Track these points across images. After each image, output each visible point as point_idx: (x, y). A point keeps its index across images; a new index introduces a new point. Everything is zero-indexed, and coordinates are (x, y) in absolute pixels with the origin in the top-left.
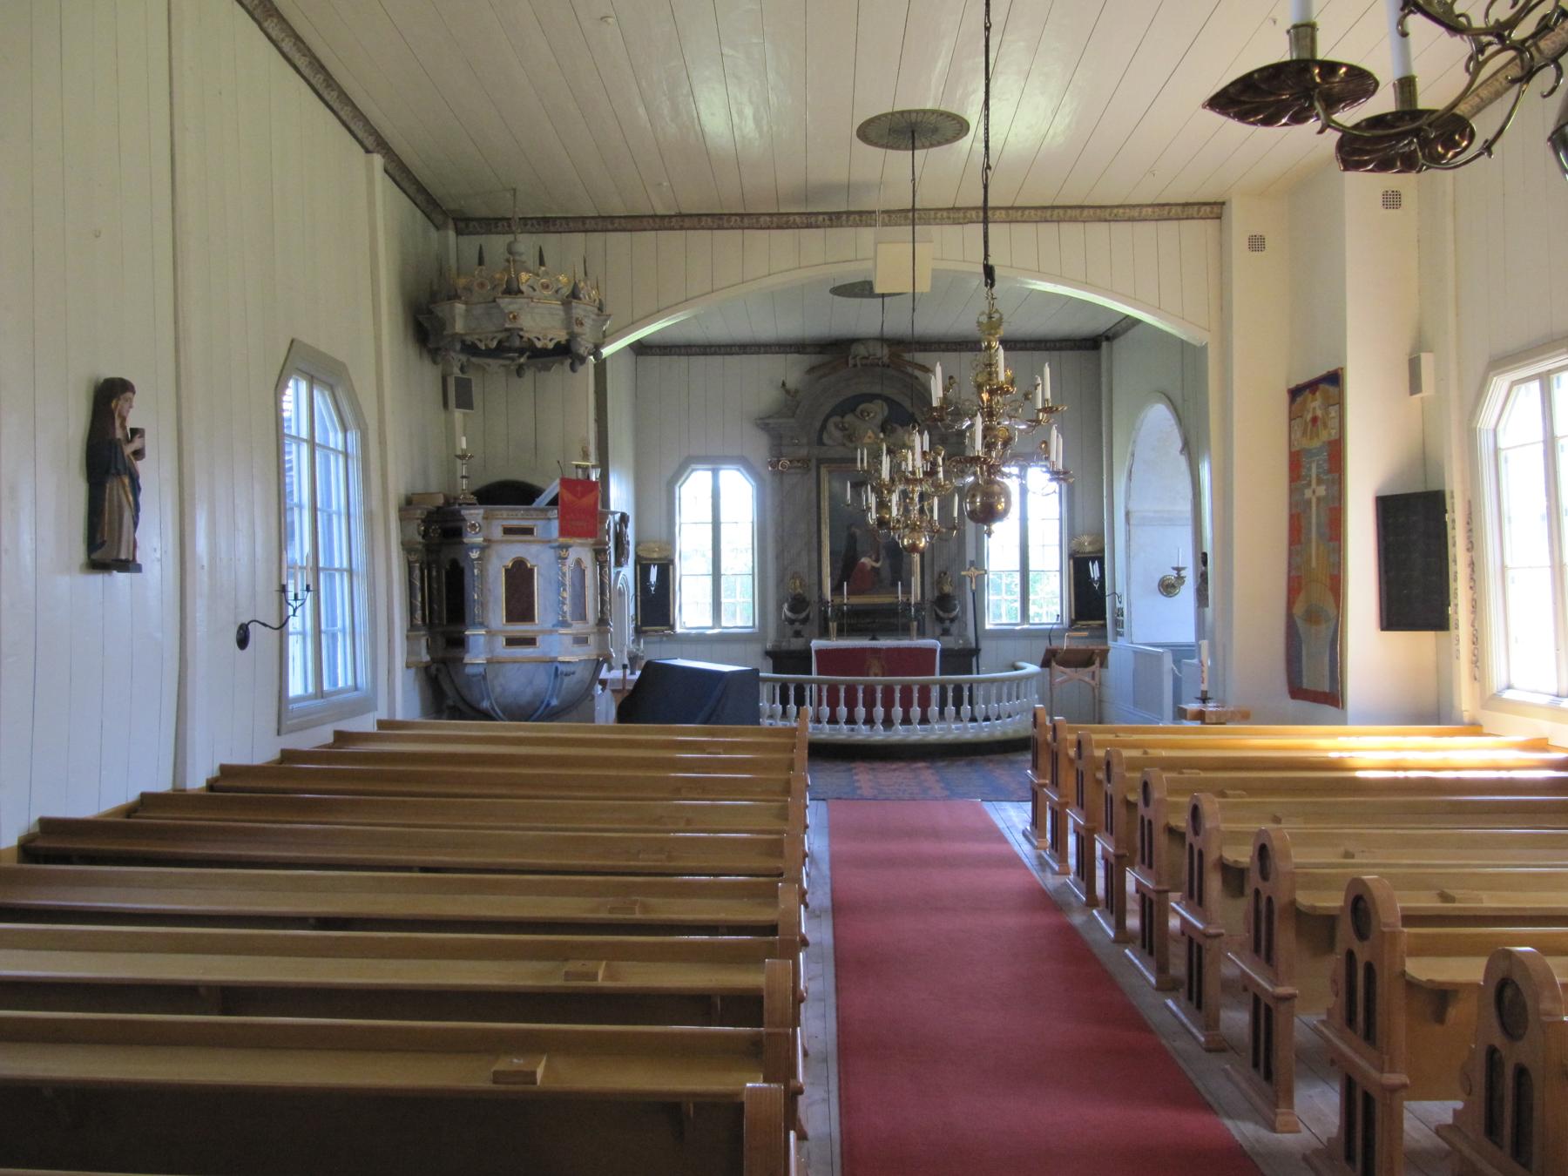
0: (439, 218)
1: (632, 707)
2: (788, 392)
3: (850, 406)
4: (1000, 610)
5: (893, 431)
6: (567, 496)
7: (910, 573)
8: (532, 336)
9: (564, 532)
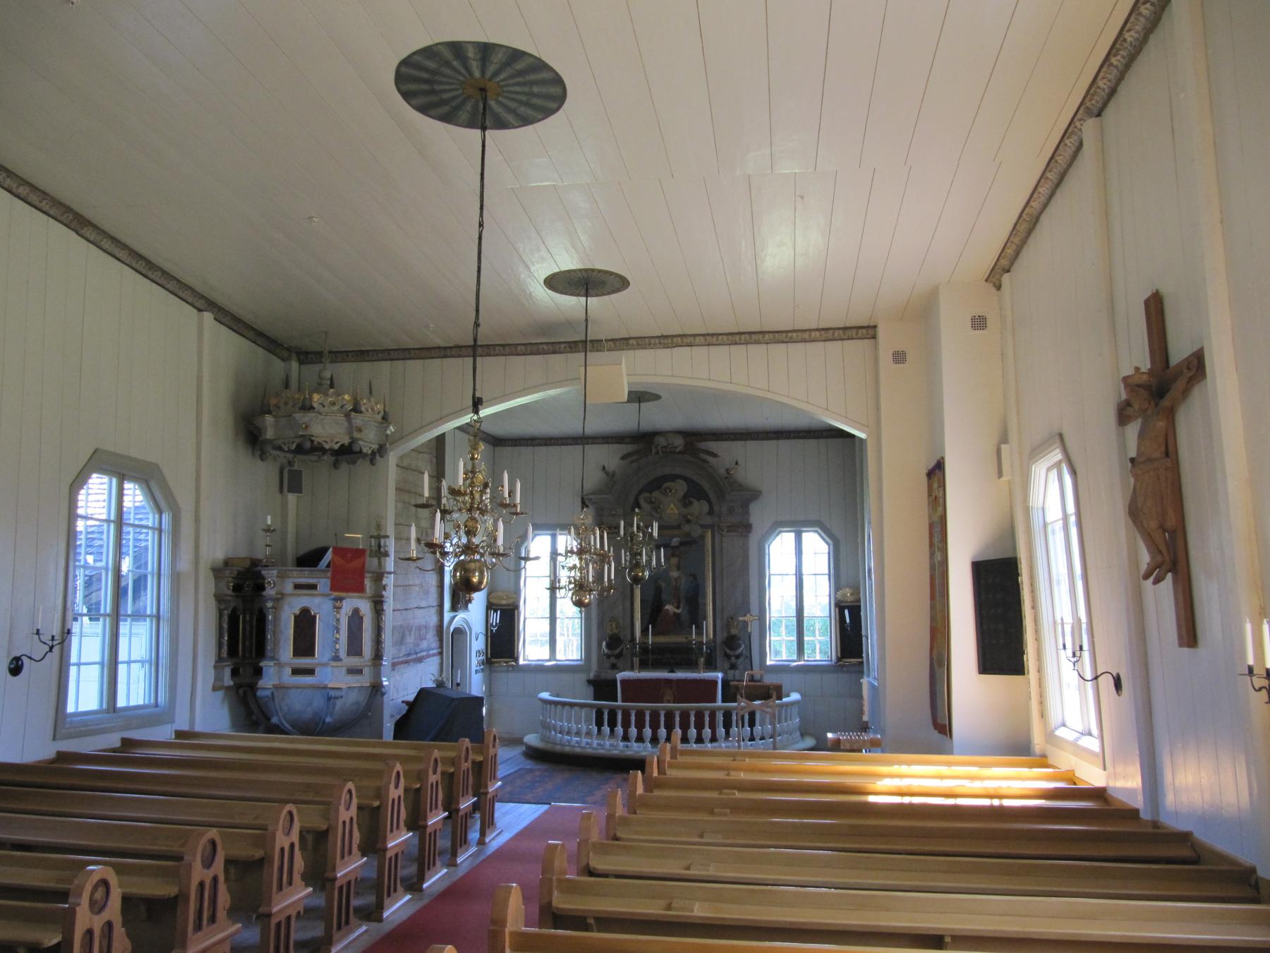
1: (404, 728)
2: (607, 474)
3: (657, 484)
4: (779, 648)
5: (691, 503)
7: (705, 618)
8: (320, 440)
9: (334, 588)
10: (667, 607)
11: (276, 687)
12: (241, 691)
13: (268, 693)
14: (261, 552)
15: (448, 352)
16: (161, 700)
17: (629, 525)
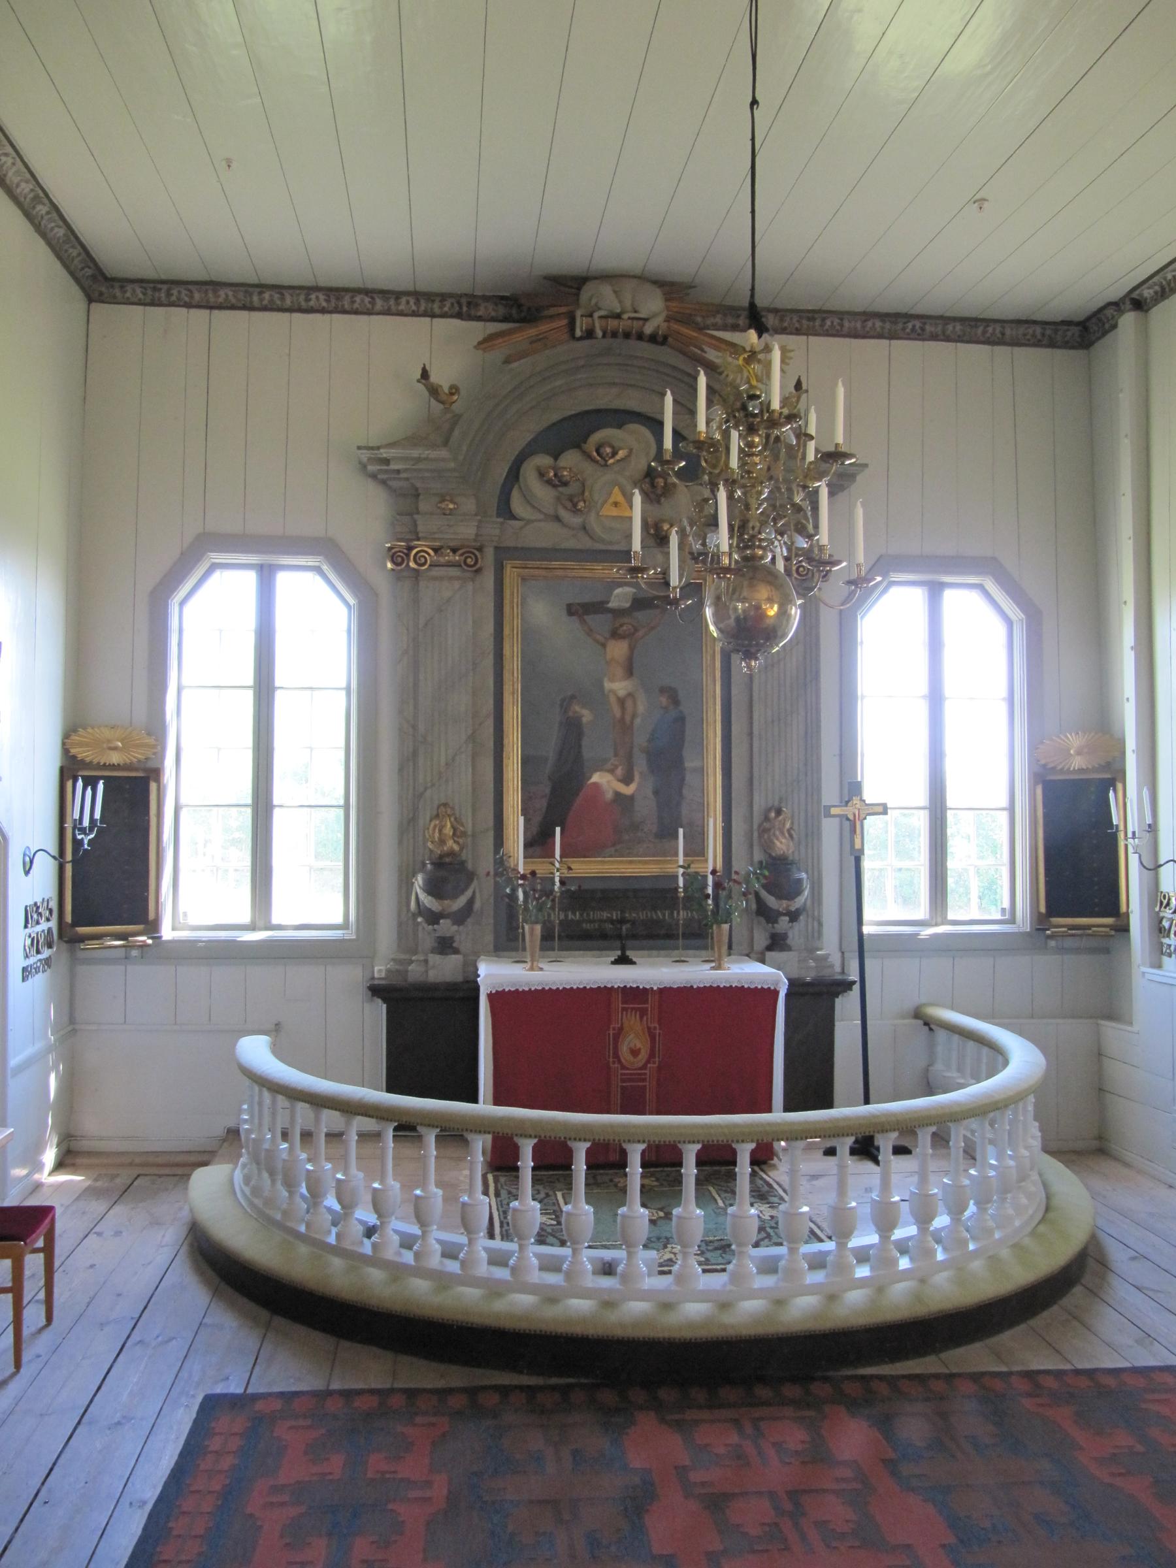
2: (434, 391)
3: (573, 433)
10: (596, 778)
17: (686, 408)
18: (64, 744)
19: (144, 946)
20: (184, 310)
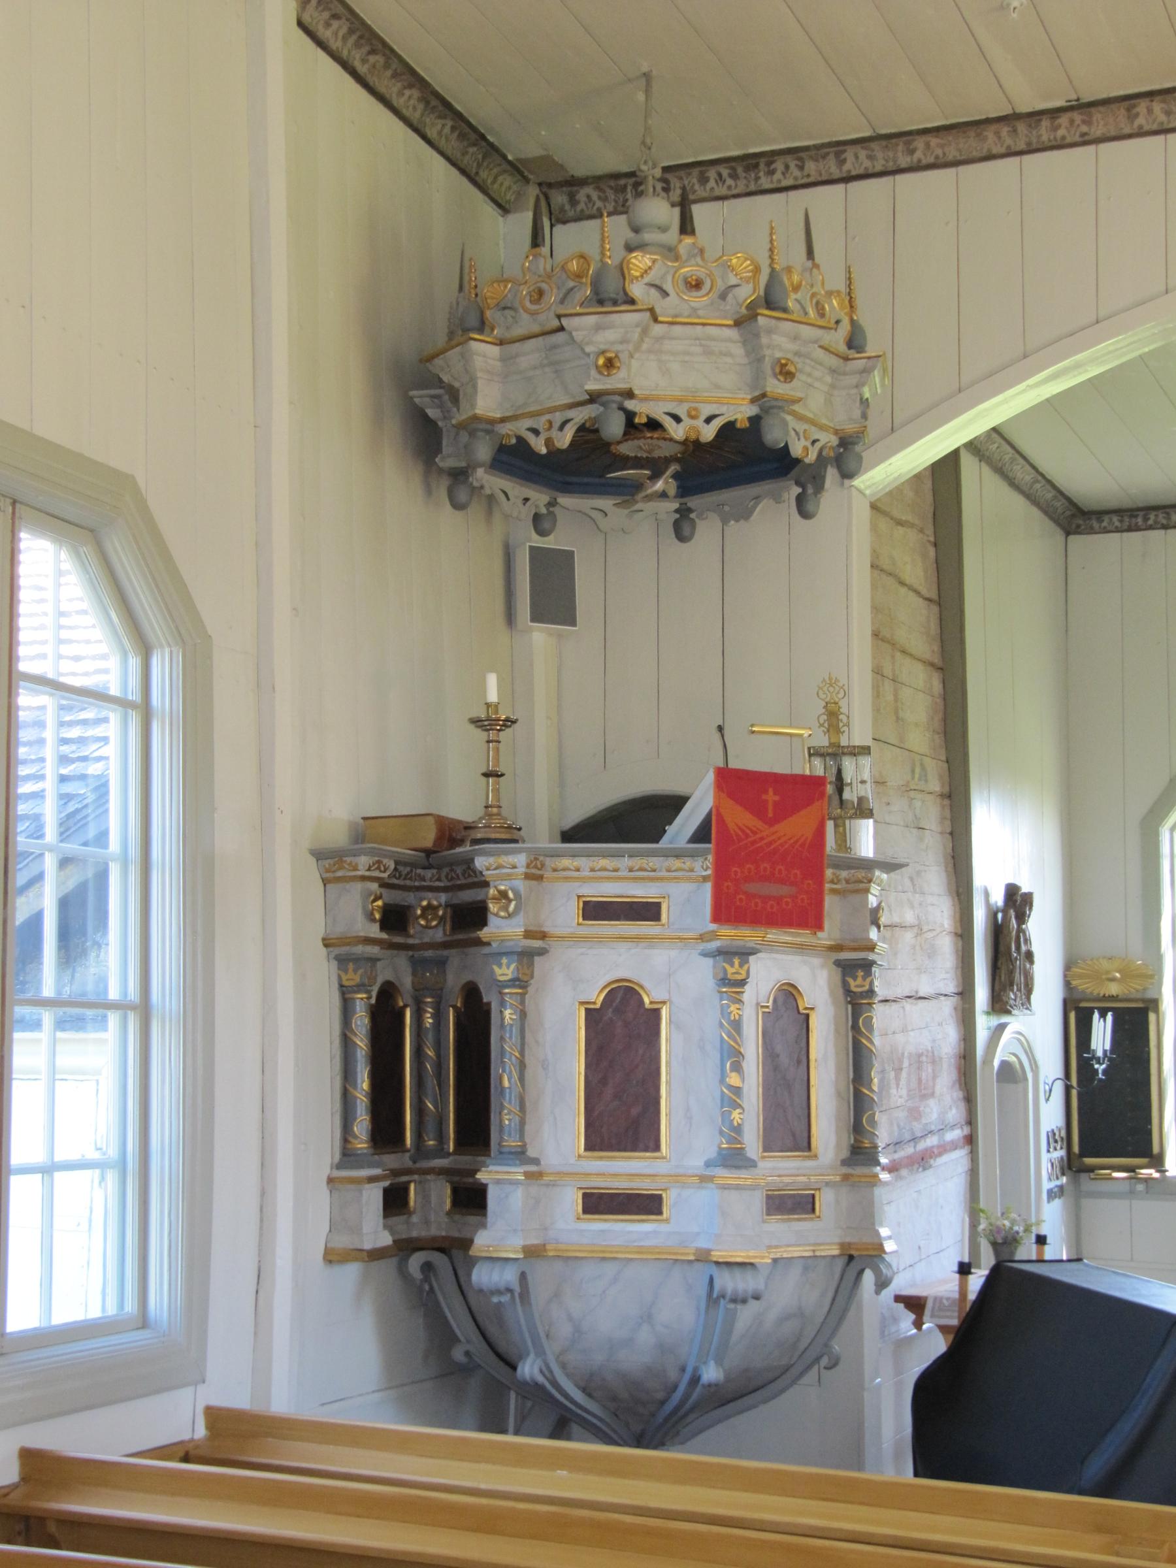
0: (506, 184)
6: (739, 818)
11: (533, 1253)
12: (416, 1261)
13: (508, 1276)
14: (462, 804)
15: (1044, 132)
16: (160, 1300)
18: (1065, 976)
19: (1148, 1180)
20: (1163, 532)
